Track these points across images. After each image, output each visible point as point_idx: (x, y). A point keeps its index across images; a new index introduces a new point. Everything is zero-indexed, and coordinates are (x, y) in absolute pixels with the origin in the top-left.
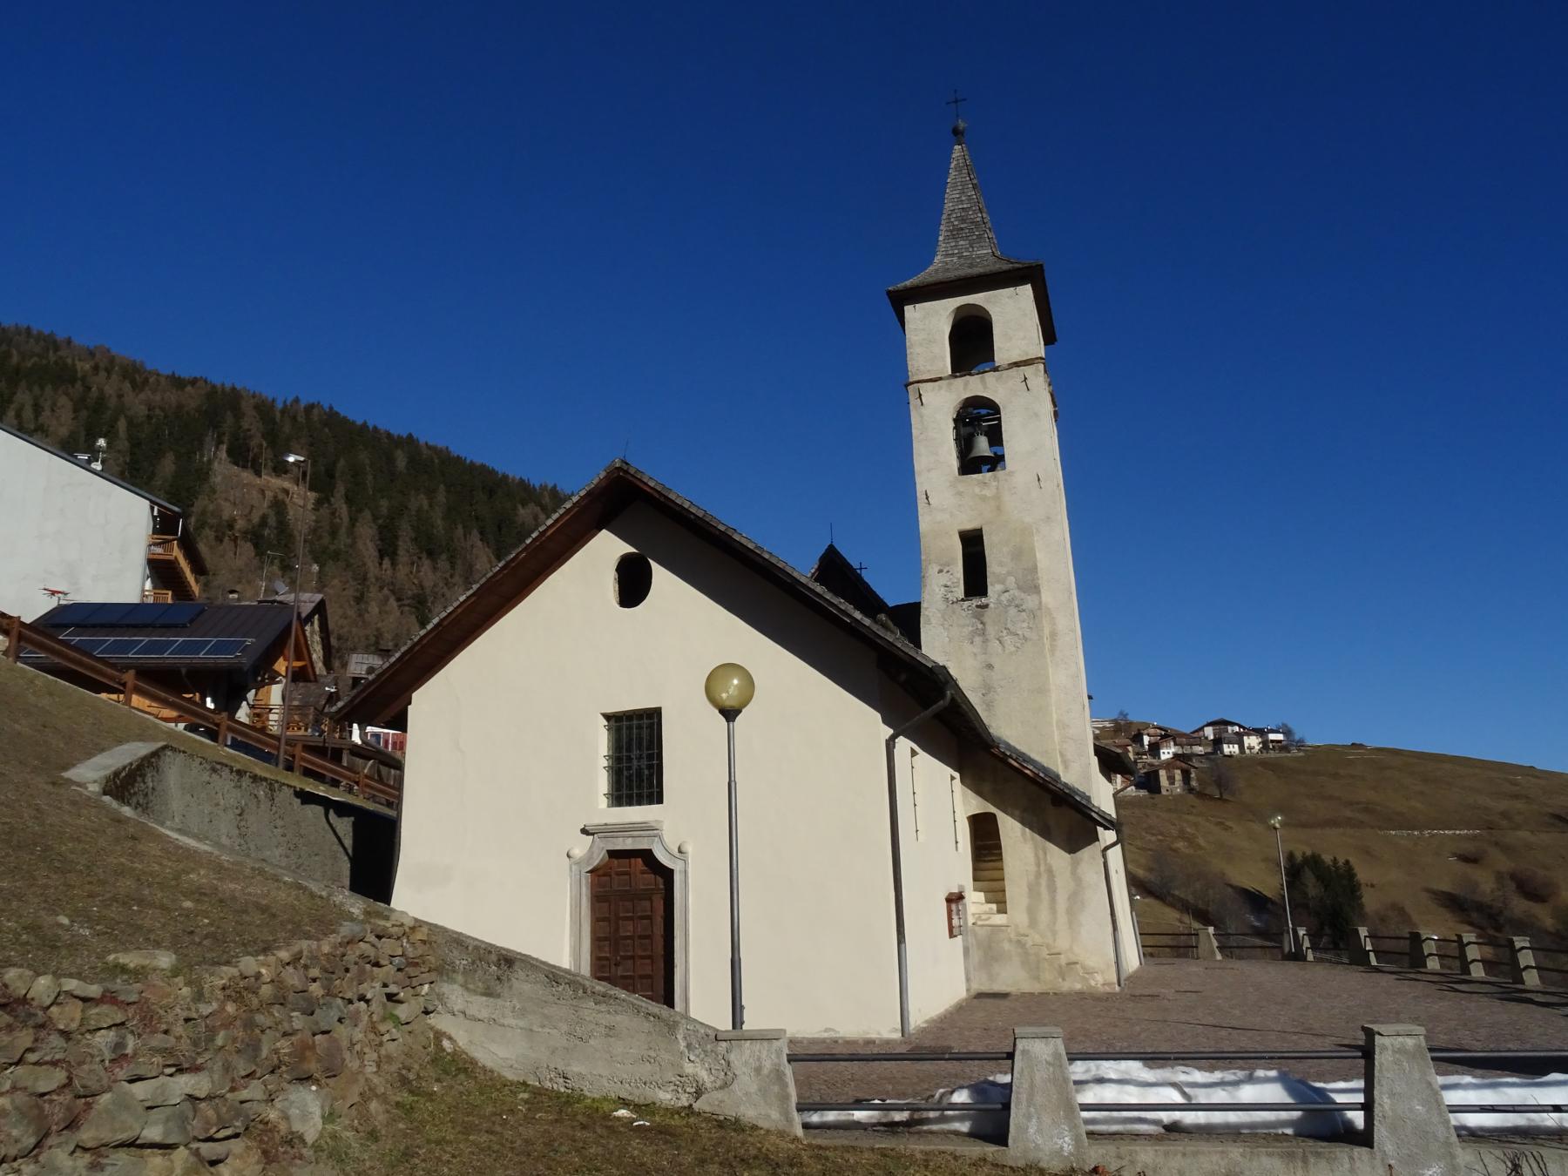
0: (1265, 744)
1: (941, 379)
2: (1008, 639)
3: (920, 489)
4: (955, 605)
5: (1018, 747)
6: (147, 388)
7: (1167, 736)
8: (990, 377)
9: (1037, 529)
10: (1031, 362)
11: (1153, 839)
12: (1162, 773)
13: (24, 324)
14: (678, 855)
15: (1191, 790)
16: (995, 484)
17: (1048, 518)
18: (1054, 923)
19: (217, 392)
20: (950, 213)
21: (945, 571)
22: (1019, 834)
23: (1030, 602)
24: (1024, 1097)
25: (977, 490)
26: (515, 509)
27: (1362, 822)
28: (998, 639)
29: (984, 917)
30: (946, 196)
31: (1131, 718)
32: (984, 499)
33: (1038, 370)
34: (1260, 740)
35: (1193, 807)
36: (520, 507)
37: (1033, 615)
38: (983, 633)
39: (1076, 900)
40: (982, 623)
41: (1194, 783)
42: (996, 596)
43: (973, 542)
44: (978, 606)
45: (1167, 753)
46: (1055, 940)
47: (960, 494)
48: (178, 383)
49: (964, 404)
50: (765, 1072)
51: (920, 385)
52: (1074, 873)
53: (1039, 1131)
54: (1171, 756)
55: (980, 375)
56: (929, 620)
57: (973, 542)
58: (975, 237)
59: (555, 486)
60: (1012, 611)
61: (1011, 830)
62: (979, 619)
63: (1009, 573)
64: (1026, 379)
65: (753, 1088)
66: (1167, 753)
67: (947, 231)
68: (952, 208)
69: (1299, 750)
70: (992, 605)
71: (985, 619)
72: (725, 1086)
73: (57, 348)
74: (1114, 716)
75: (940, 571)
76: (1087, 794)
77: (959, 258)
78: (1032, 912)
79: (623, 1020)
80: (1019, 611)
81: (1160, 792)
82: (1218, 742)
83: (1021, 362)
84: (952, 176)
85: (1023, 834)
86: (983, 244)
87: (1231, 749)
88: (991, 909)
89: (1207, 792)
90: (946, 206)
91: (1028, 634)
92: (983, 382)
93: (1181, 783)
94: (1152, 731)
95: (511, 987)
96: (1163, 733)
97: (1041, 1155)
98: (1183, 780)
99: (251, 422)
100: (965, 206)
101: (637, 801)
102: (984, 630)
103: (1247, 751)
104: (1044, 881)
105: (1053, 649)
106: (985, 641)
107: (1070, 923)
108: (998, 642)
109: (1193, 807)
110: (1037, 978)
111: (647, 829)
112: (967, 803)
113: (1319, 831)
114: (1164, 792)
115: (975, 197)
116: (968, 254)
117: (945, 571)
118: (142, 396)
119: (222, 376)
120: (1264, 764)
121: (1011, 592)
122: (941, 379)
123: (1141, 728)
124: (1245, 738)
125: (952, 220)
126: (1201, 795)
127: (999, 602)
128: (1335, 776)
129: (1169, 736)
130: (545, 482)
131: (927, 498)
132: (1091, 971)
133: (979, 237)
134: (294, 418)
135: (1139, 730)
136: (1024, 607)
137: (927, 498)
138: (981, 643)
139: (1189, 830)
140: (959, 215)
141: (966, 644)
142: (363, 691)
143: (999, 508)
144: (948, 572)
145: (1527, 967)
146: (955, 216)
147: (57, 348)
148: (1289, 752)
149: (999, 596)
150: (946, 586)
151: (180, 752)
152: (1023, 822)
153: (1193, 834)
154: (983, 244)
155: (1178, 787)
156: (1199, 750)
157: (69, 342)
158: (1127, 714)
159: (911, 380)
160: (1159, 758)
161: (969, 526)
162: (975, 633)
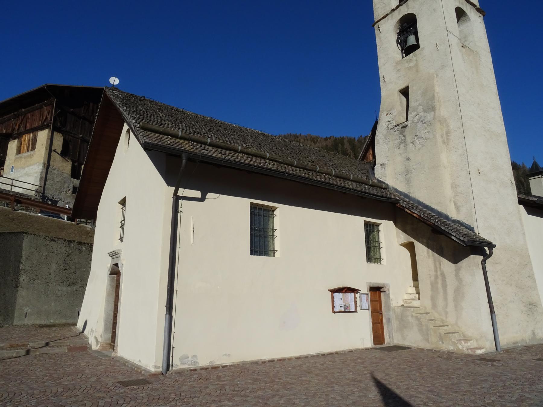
1: (387, 15)
3: (381, 76)
4: (391, 130)
5: (424, 202)
6: (317, 142)
9: (437, 75)
13: (289, 133)
18: (446, 308)
19: (337, 139)
21: (389, 113)
22: (426, 253)
23: (429, 116)
29: (408, 301)
32: (410, 68)
37: (430, 124)
38: (404, 141)
39: (459, 292)
40: (404, 136)
44: (402, 128)
46: (447, 318)
47: (399, 71)
48: (326, 139)
52: (457, 275)
60: (419, 125)
61: (421, 249)
62: (402, 135)
63: (420, 105)
70: (409, 125)
71: (405, 134)
73: (298, 137)
75: (387, 114)
76: (471, 226)
78: (433, 299)
80: (423, 124)
85: (428, 253)
88: (415, 297)
92: (408, 7)
99: (347, 146)
102: (405, 139)
104: (440, 281)
105: (446, 142)
107: (456, 306)
108: (412, 144)
110: (427, 340)
112: (404, 238)
118: (317, 145)
119: (338, 135)
121: (420, 114)
122: (387, 15)
127: (413, 121)
132: (468, 339)
134: (361, 142)
136: (425, 121)
138: (404, 147)
143: (417, 71)
144: (390, 114)
147: (298, 137)
149: (414, 118)
151: (31, 234)
152: (428, 246)
157: (300, 135)
159: (376, 20)
162: (400, 143)
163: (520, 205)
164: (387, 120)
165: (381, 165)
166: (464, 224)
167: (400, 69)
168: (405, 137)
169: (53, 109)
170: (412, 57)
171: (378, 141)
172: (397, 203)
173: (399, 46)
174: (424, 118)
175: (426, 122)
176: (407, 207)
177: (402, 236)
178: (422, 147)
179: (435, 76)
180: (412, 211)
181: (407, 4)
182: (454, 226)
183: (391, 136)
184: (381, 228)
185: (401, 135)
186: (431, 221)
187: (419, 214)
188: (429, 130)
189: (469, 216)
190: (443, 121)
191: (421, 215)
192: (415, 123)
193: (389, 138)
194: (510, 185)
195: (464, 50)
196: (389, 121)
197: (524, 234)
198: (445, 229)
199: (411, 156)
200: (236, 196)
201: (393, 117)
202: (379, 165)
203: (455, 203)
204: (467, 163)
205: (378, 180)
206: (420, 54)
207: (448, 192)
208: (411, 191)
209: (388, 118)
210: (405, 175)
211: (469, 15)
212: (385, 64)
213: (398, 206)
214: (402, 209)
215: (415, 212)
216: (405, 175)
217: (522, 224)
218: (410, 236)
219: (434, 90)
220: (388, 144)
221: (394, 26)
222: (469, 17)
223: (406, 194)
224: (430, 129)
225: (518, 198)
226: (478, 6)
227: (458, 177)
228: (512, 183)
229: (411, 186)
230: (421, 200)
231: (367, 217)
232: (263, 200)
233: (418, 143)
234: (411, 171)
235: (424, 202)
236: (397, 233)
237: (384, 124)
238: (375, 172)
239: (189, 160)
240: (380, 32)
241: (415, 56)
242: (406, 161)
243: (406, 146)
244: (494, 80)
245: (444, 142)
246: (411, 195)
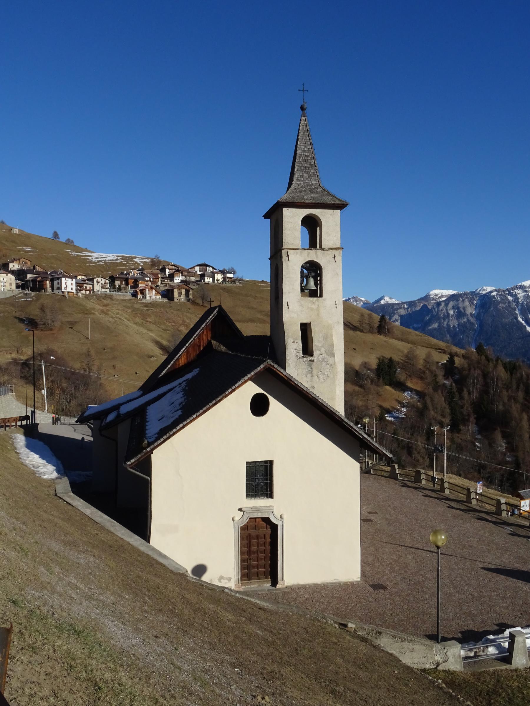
0: (225, 279)
1: (298, 249)
2: (321, 376)
4: (300, 359)
7: (179, 270)
11: (170, 324)
12: (176, 291)
14: (280, 519)
15: (189, 300)
16: (317, 303)
17: (338, 322)
21: (296, 342)
24: (516, 652)
25: (310, 305)
27: (265, 321)
31: (160, 259)
32: (312, 309)
33: (340, 253)
34: (222, 276)
35: (189, 309)
38: (311, 373)
40: (311, 368)
41: (191, 297)
43: (305, 329)
44: (310, 361)
45: (178, 279)
47: (302, 305)
50: (456, 656)
53: (519, 660)
54: (179, 281)
56: (290, 365)
57: (305, 329)
60: (324, 364)
63: (322, 346)
65: (453, 661)
66: (178, 279)
69: (240, 283)
70: (315, 361)
72: (445, 661)
74: (153, 257)
75: (294, 342)
79: (417, 647)
81: (174, 300)
82: (203, 276)
87: (209, 280)
89: (196, 301)
91: (329, 374)
92: (316, 254)
93: (185, 296)
94: (170, 267)
95: (380, 641)
96: (176, 269)
97: (519, 665)
98: (186, 294)
102: (312, 371)
103: (216, 281)
106: (312, 376)
109: (189, 309)
111: (269, 509)
113: (246, 324)
114: (176, 300)
117: (296, 342)
120: (224, 289)
121: (323, 355)
122: (298, 249)
123: (165, 265)
124: (216, 275)
126: (194, 303)
127: (318, 359)
128: (255, 297)
129: (180, 271)
131: (288, 306)
135: (164, 266)
136: (328, 363)
137: (288, 306)
139: (187, 321)
142: (144, 455)
143: (318, 315)
145: (473, 498)
148: (235, 284)
150: (296, 349)
153: (189, 323)
155: (183, 298)
156: (193, 279)
158: (159, 257)
160: (174, 282)
161: (305, 321)
164: (295, 348)
169: (178, 359)
241: (318, 301)
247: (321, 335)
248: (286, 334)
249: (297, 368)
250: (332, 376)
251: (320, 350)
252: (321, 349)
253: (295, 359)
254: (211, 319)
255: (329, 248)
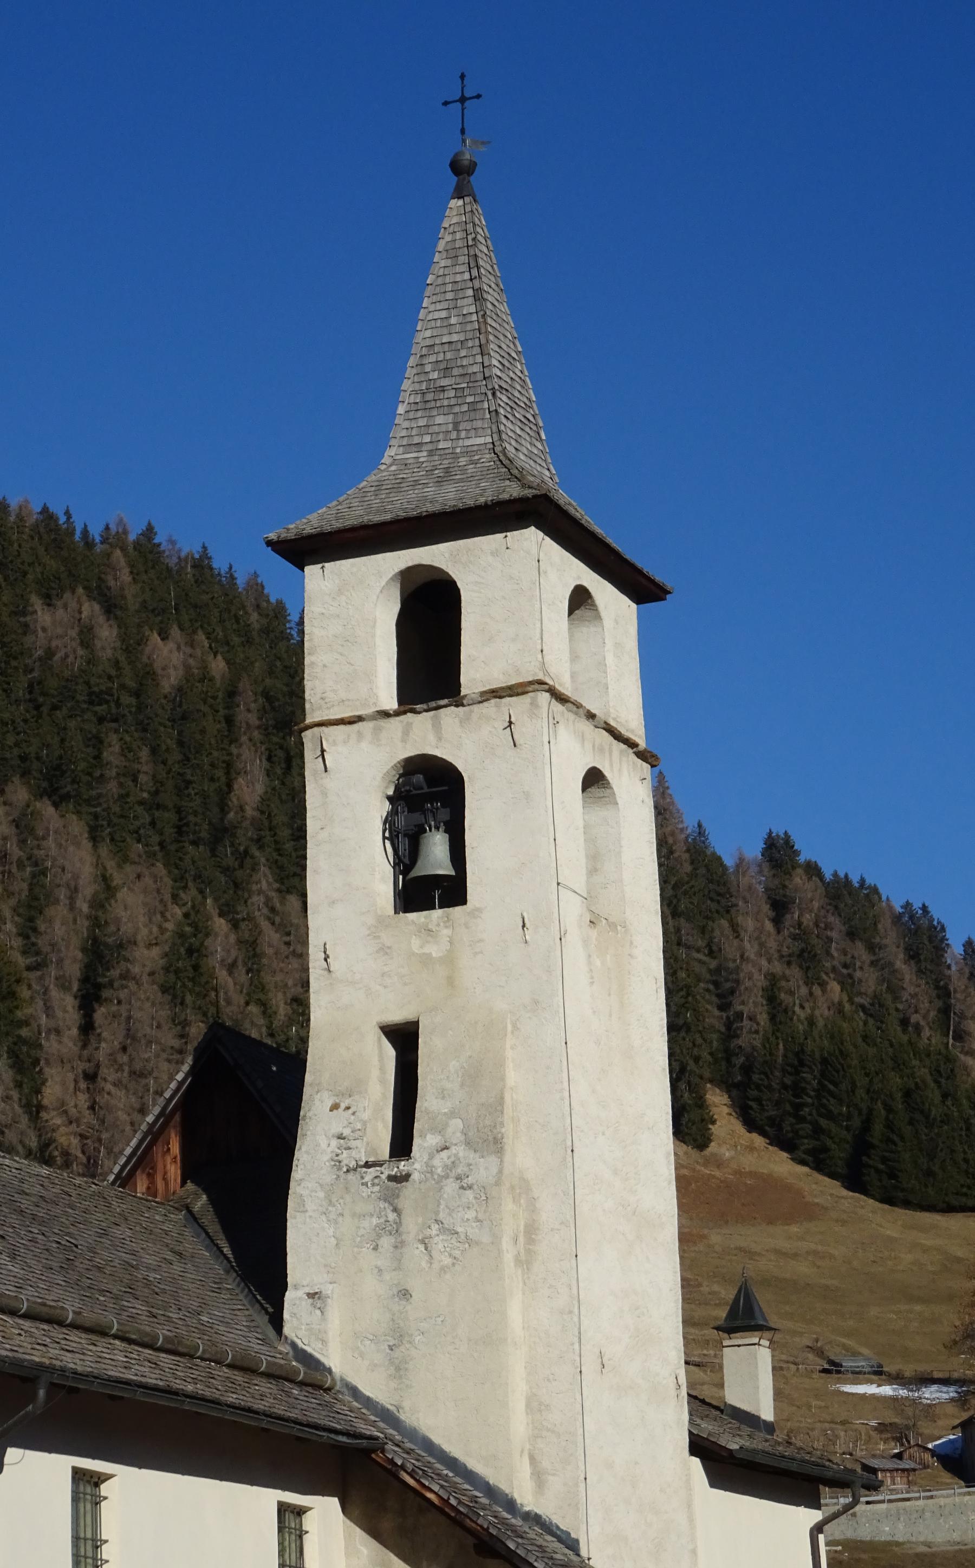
1: (360, 719)
2: (439, 1243)
4: (350, 1176)
5: (446, 1447)
8: (449, 715)
9: (515, 1028)
10: (520, 690)
16: (446, 932)
17: (536, 1002)
20: (424, 351)
21: (343, 1106)
25: (415, 944)
26: (22, 611)
28: (422, 1242)
30: (421, 316)
32: (426, 960)
36: (37, 603)
37: (486, 1197)
38: (396, 1230)
40: (395, 1210)
42: (426, 1158)
44: (392, 1178)
47: (384, 950)
49: (404, 767)
51: (324, 729)
55: (432, 713)
58: (465, 408)
59: (149, 531)
60: (451, 1187)
62: (392, 1205)
63: (452, 1114)
64: (510, 723)
67: (415, 392)
68: (428, 342)
70: (415, 1176)
75: (335, 1107)
76: (573, 1535)
77: (431, 453)
80: (462, 1188)
83: (502, 689)
84: (436, 269)
86: (479, 424)
90: (419, 337)
91: (473, 1231)
92: (437, 726)
100: (455, 338)
101: (830, 1551)
102: (399, 1224)
105: (525, 1262)
108: (422, 1247)
115: (474, 317)
116: (447, 444)
117: (343, 1106)
121: (453, 1150)
122: (360, 719)
125: (428, 368)
127: (430, 1170)
130: (120, 522)
133: (473, 408)
136: (470, 1180)
138: (392, 1249)
140: (441, 357)
141: (366, 1250)
143: (451, 981)
144: (348, 1108)
146: (433, 358)
149: (431, 1157)
150: (340, 1137)
154: (479, 424)
162: (382, 1230)
163: (693, 1458)
164: (337, 1128)
165: (311, 1296)
166: (554, 1529)
167: (389, 948)
168: (399, 1215)
170: (438, 925)
171: (302, 1203)
172: (374, 1451)
173: (388, 843)
174: (466, 1169)
175: (472, 1184)
176: (409, 1467)
177: (365, 1551)
178: (454, 1264)
179: (509, 1027)
180: (423, 1481)
181: (435, 717)
182: (532, 1535)
183: (348, 1198)
184: (310, 1522)
185: (387, 1205)
186: (479, 1522)
187: (441, 1493)
188: (480, 1216)
189: (569, 1505)
190: (523, 1188)
191: (451, 1498)
192: (436, 1177)
193: (341, 1201)
194: (673, 1392)
195: (593, 933)
196: (344, 1139)
197: (694, 1552)
198: (517, 1548)
199: (416, 1286)
200: (50, 1452)
201: (359, 1126)
202: (301, 1293)
203: (532, 1459)
204: (576, 1339)
205: (294, 1345)
206: (467, 926)
207: (519, 1425)
208: (406, 1404)
209: (338, 1123)
210: (389, 1346)
211: (614, 786)
212: (333, 902)
213: (379, 1460)
214: (392, 1470)
215: (433, 1488)
216: (389, 1346)
217: (691, 1520)
218: (392, 1551)
219: (503, 1079)
220: (336, 1222)
221: (381, 775)
222: (614, 794)
223: (388, 1410)
224: (485, 1212)
225: (690, 1433)
226: (642, 744)
227: (548, 1380)
228: (679, 1386)
229: (407, 1386)
230: (437, 1439)
231: (284, 1488)
232: (94, 1457)
233: (440, 1246)
234: (412, 1335)
235: (443, 1447)
236: (348, 1538)
237: (323, 1142)
238: (286, 1315)
239: (53, 1386)
240: (326, 771)
241: (448, 919)
242: (397, 1299)
243: (402, 1247)
244: (662, 1020)
245: (518, 1261)
246: (402, 1417)
247: (453, 1065)
248: (308, 1078)
249: (332, 1216)
250: (486, 1239)
251: (441, 1131)
252: (447, 1125)
253: (329, 1178)
254: (181, 1084)
255: (483, 694)
